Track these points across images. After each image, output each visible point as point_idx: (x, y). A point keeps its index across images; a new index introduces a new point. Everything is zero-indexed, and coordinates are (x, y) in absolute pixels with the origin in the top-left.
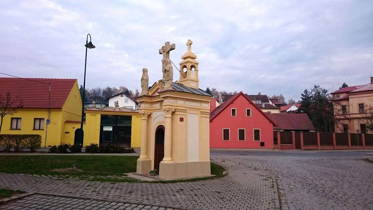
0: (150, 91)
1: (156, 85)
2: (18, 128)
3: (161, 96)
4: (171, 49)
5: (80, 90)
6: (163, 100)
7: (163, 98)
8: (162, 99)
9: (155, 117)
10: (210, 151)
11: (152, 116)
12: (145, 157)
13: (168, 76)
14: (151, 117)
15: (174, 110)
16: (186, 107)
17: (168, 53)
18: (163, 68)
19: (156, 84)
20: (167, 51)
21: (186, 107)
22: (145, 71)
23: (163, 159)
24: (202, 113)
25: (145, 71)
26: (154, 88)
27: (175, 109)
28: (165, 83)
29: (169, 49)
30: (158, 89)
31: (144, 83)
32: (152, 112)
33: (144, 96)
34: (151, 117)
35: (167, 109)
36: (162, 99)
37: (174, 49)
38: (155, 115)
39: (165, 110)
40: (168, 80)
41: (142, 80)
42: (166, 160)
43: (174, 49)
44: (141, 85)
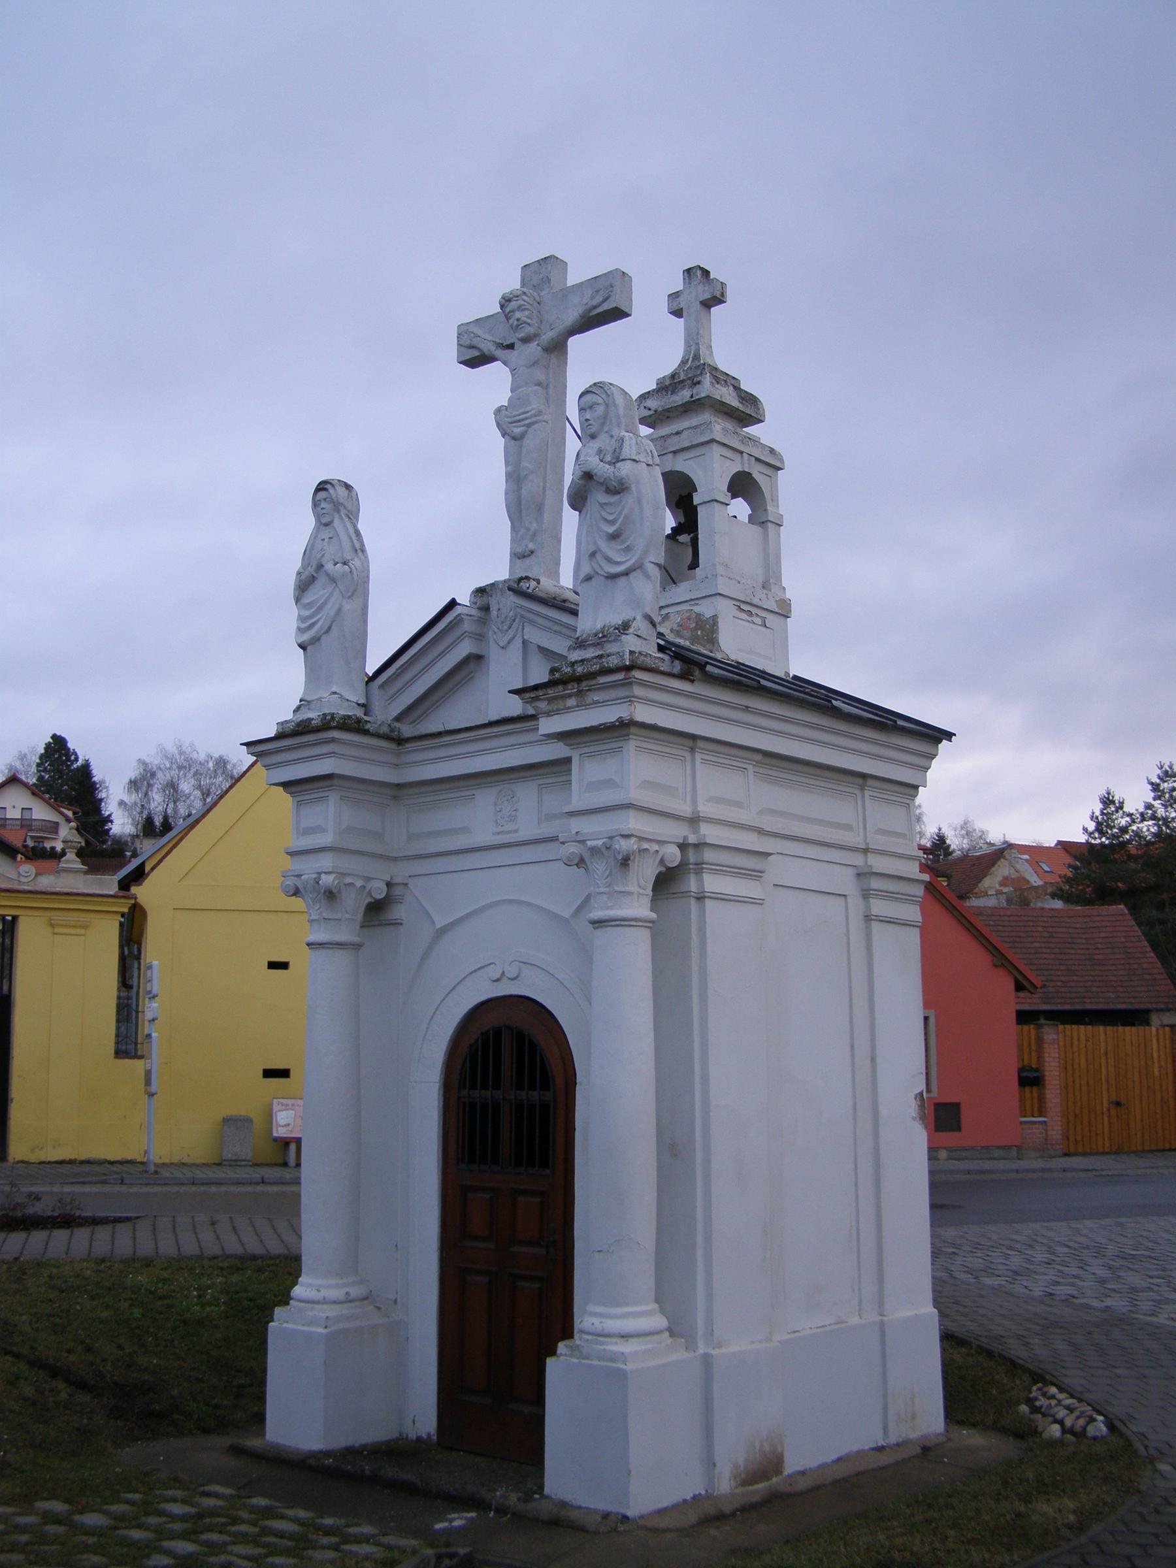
0: (382, 686)
1: (457, 633)
2: (139, 1053)
3: (548, 725)
4: (591, 321)
5: (668, 537)
6: (568, 761)
7: (564, 736)
8: (558, 750)
9: (440, 923)
10: (299, 1183)
11: (399, 912)
12: (338, 1293)
13: (614, 537)
14: (397, 924)
15: (673, 855)
16: (760, 832)
17: (558, 348)
18: (509, 476)
19: (459, 620)
20: (548, 336)
21: (760, 832)
22: (333, 501)
23: (297, 1291)
24: (875, 883)
25: (333, 501)
26: (441, 647)
27: (683, 846)
28: (575, 613)
29: (572, 315)
30: (472, 666)
31: (330, 610)
32: (400, 872)
33: (328, 724)
34: (397, 924)
35: (624, 845)
36: (558, 750)
37: (627, 315)
38: (435, 898)
39: (594, 851)
40: (613, 577)
41: (304, 585)
42: (616, 1314)
43: (618, 314)
44: (300, 630)
